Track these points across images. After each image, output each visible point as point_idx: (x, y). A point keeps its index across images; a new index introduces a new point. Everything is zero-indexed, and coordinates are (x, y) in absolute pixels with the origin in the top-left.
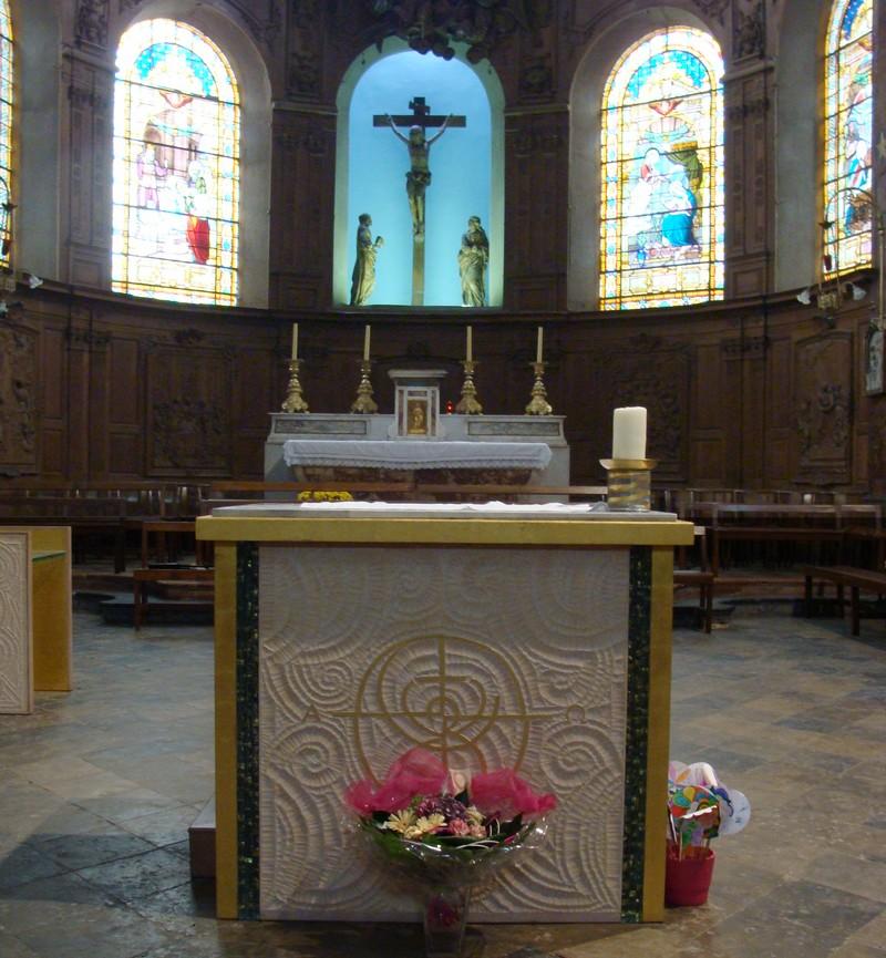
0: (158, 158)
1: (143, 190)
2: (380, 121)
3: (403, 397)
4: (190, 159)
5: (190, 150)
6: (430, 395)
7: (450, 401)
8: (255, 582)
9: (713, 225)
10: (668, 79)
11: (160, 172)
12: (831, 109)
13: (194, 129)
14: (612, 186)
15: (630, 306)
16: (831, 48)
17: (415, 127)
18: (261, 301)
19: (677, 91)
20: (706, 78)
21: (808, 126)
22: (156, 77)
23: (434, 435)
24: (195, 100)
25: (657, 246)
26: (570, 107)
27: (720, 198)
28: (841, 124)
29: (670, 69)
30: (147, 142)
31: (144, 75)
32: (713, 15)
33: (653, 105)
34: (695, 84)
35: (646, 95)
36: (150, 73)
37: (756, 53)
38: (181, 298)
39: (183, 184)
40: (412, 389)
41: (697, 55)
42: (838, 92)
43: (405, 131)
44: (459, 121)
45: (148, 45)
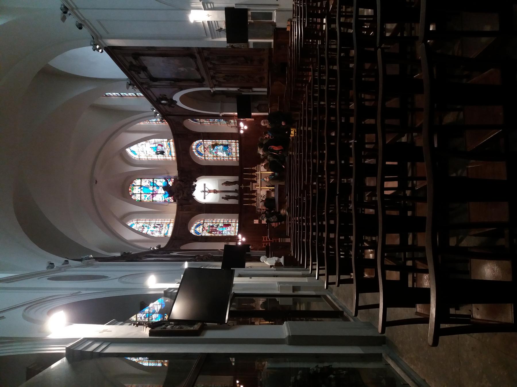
3: (254, 189)
9: (225, 142)
15: (238, 155)
19: (203, 147)
25: (228, 151)
27: (221, 141)
28: (212, 122)
33: (205, 151)
44: (205, 185)
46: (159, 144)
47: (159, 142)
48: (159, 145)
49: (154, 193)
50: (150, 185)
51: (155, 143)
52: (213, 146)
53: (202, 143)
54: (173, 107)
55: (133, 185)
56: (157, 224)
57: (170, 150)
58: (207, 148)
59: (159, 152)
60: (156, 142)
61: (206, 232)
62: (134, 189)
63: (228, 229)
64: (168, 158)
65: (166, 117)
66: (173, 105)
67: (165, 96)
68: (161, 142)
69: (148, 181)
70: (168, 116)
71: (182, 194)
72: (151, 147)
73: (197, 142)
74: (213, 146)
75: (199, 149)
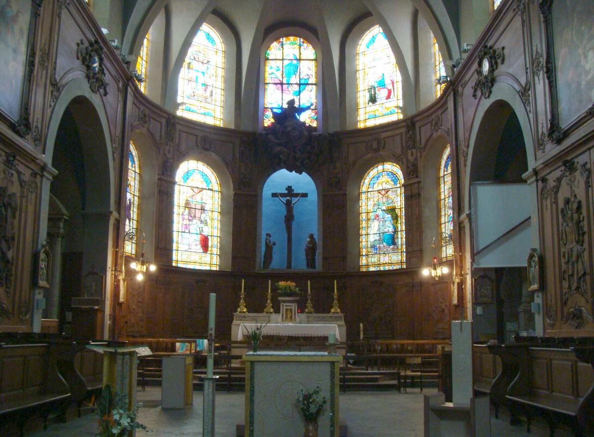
0: (189, 213)
1: (184, 225)
2: (274, 195)
3: (283, 307)
4: (201, 213)
5: (201, 209)
6: (293, 306)
7: (302, 309)
8: (254, 370)
9: (401, 238)
10: (385, 182)
11: (190, 218)
12: (442, 197)
13: (203, 201)
14: (364, 222)
15: (372, 269)
16: (442, 174)
17: (288, 198)
18: (228, 269)
20: (398, 182)
21: (434, 203)
22: (190, 183)
23: (295, 321)
24: (204, 190)
25: (382, 246)
28: (446, 202)
29: (385, 178)
30: (185, 207)
31: (185, 181)
32: (399, 160)
33: (379, 192)
34: (394, 184)
35: (376, 187)
36: (187, 181)
37: (415, 176)
38: (198, 267)
39: (199, 222)
41: (395, 173)
42: (444, 191)
43: (284, 200)
45: (187, 171)
46: (392, 90)
47: (395, 90)
48: (390, 92)
50: (301, 78)
51: (393, 83)
52: (392, 211)
53: (398, 185)
54: (474, 96)
55: (301, 43)
59: (375, 93)
60: (395, 84)
62: (293, 47)
63: (196, 245)
65: (451, 87)
66: (479, 93)
67: (499, 61)
68: (396, 95)
69: (310, 73)
70: (452, 93)
71: (278, 141)
72: (383, 75)
73: (400, 174)
74: (392, 211)
75: (385, 178)
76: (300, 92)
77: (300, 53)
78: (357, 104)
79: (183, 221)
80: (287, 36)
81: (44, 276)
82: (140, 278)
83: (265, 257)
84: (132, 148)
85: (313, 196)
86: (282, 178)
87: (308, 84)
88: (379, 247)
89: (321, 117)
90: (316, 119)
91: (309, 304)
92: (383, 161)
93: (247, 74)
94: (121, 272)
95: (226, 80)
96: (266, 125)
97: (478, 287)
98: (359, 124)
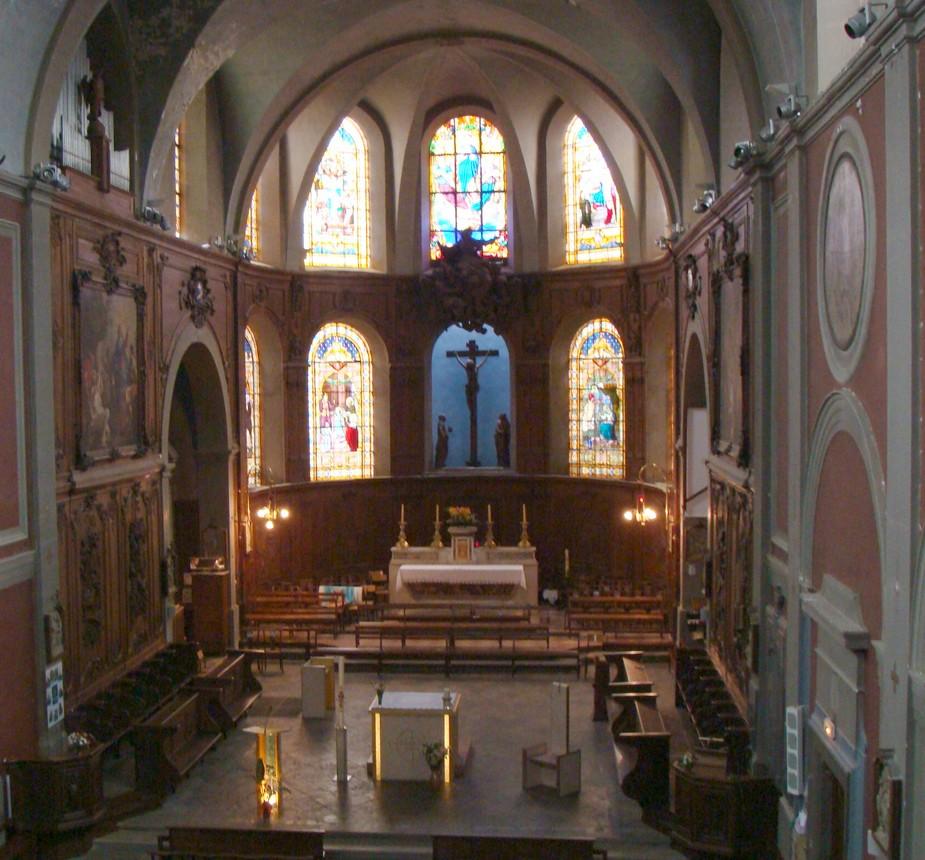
0: (330, 399)
2: (450, 354)
3: (456, 541)
22: (329, 357)
25: (598, 439)
26: (550, 362)
33: (595, 360)
40: (460, 538)
49: (460, 196)
52: (610, 390)
56: (352, 217)
57: (595, 248)
58: (606, 371)
59: (590, 212)
61: (330, 374)
64: (571, 237)
76: (481, 204)
77: (481, 144)
78: (565, 227)
79: (321, 411)
80: (460, 115)
81: (173, 581)
82: (270, 526)
83: (438, 449)
84: (249, 335)
85: (504, 352)
86: (455, 337)
87: (493, 192)
88: (595, 441)
89: (512, 241)
90: (507, 246)
91: (490, 536)
92: (600, 316)
93: (404, 169)
94: (273, 649)
95: (372, 196)
96: (433, 258)
97: (691, 540)
98: (567, 257)
